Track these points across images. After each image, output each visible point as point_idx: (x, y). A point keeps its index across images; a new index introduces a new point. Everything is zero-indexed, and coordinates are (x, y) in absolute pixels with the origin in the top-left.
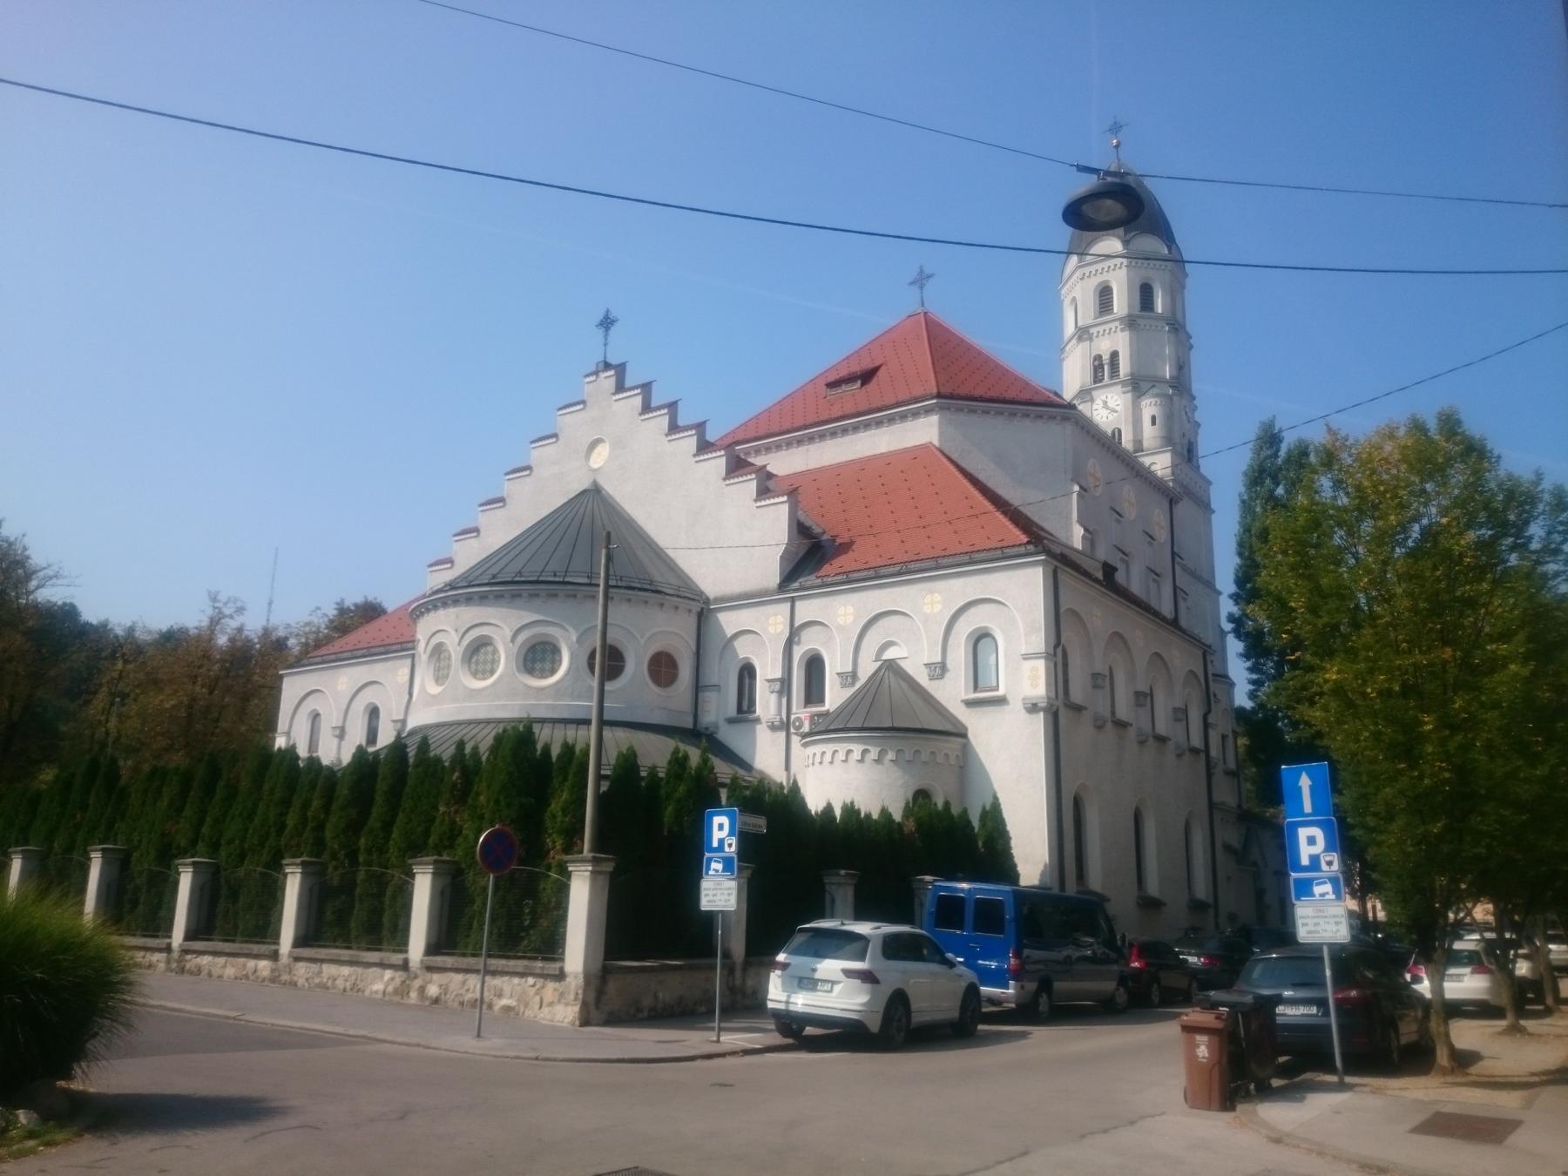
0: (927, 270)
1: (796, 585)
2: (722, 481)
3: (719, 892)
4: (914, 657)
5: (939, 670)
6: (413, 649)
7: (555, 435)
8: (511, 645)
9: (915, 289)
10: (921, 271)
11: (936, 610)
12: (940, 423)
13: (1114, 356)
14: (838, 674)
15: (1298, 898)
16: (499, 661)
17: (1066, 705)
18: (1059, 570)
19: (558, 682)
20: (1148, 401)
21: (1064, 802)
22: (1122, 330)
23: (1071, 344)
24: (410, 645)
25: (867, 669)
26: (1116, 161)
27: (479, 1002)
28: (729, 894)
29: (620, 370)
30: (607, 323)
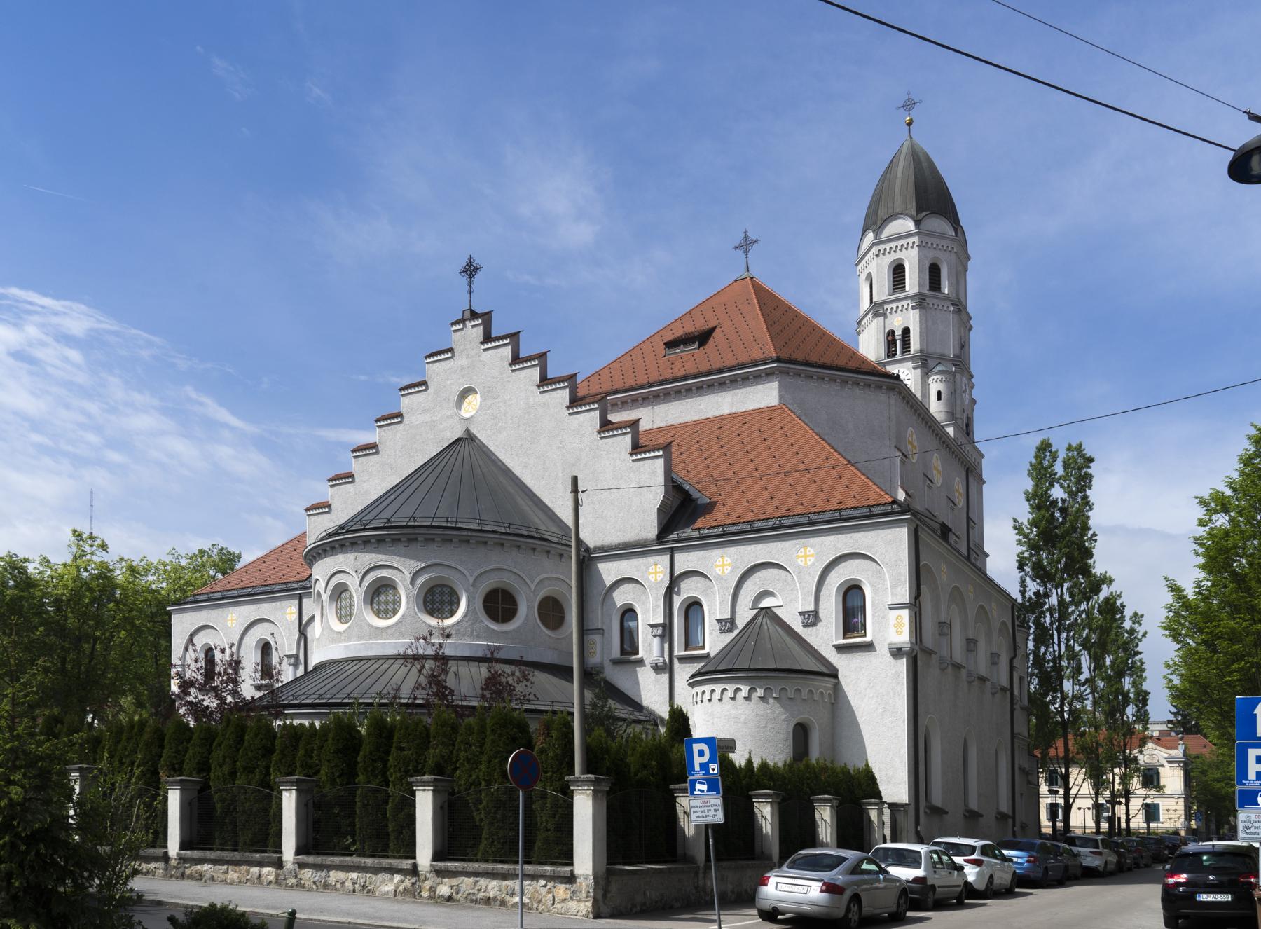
0: (752, 236)
1: (673, 536)
2: (596, 433)
3: (706, 809)
4: (790, 609)
5: (811, 618)
6: (310, 588)
7: (424, 383)
8: (411, 587)
9: (740, 253)
10: (746, 236)
11: (809, 563)
12: (780, 387)
13: (906, 331)
14: (717, 620)
15: (1241, 806)
16: (400, 602)
17: (922, 650)
18: (920, 530)
19: (457, 623)
20: (935, 377)
21: (920, 733)
22: (913, 308)
23: (867, 318)
24: (306, 584)
25: (744, 615)
26: (909, 138)
27: (519, 905)
28: (716, 810)
29: (486, 318)
30: (470, 270)
